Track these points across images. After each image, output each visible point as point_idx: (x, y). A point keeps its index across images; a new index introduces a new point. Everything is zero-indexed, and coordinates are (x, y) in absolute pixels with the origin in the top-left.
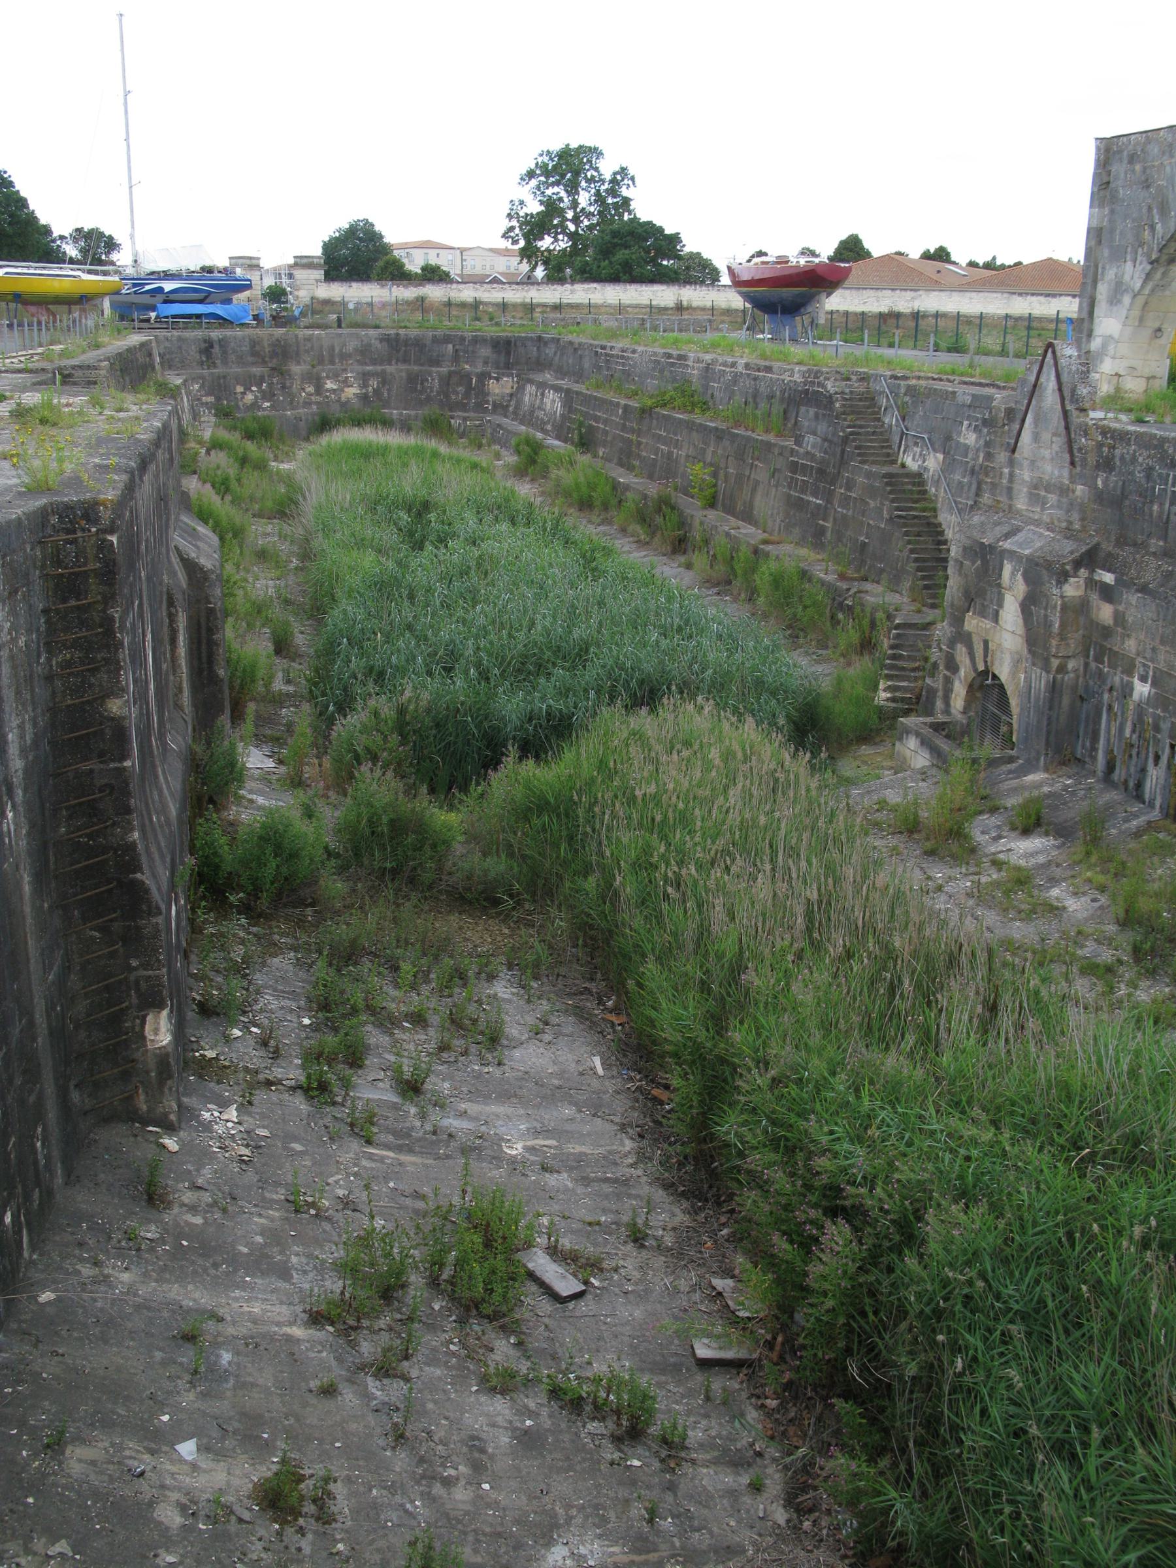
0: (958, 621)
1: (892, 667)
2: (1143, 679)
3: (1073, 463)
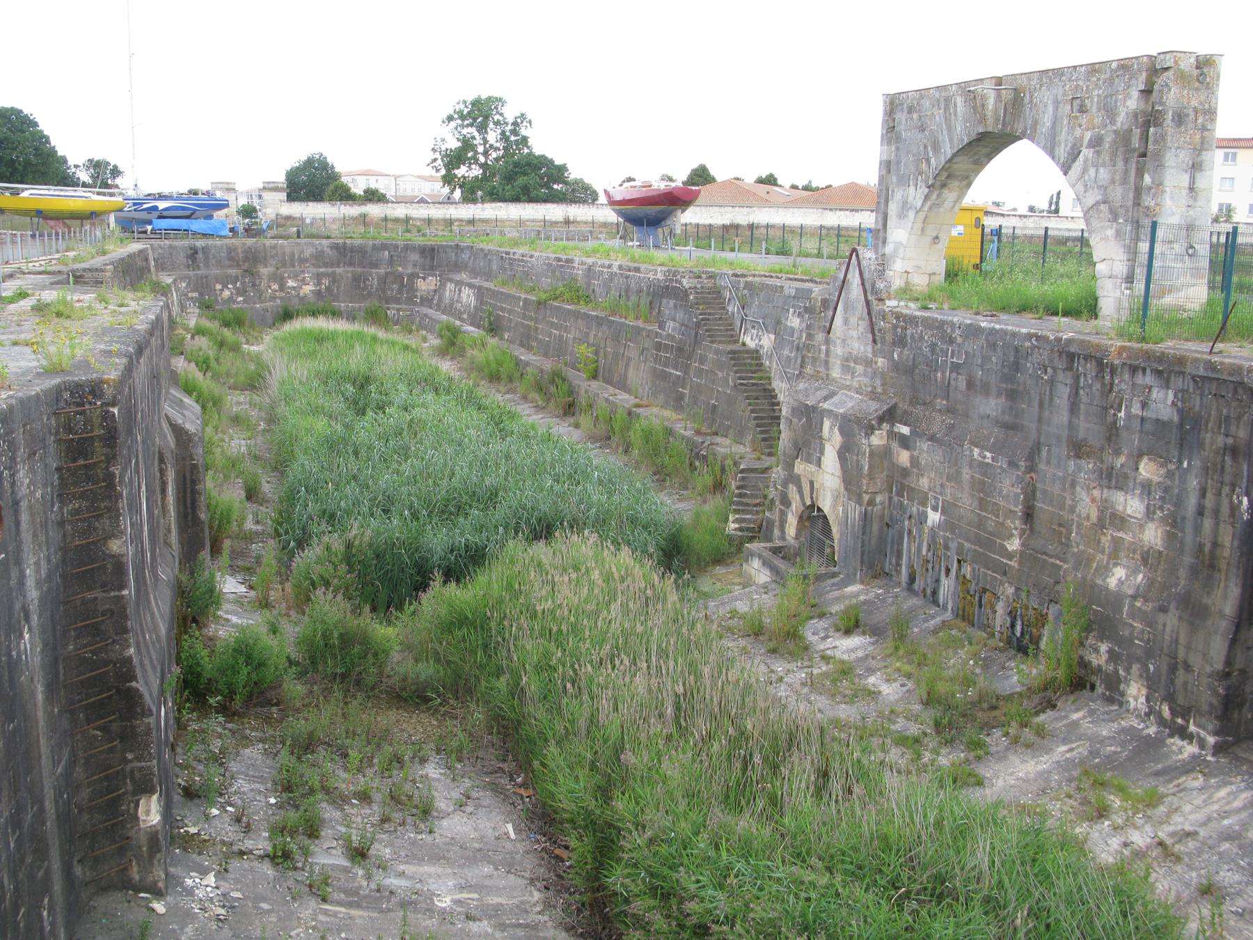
0: (790, 466)
1: (738, 503)
2: (935, 509)
3: (874, 341)
